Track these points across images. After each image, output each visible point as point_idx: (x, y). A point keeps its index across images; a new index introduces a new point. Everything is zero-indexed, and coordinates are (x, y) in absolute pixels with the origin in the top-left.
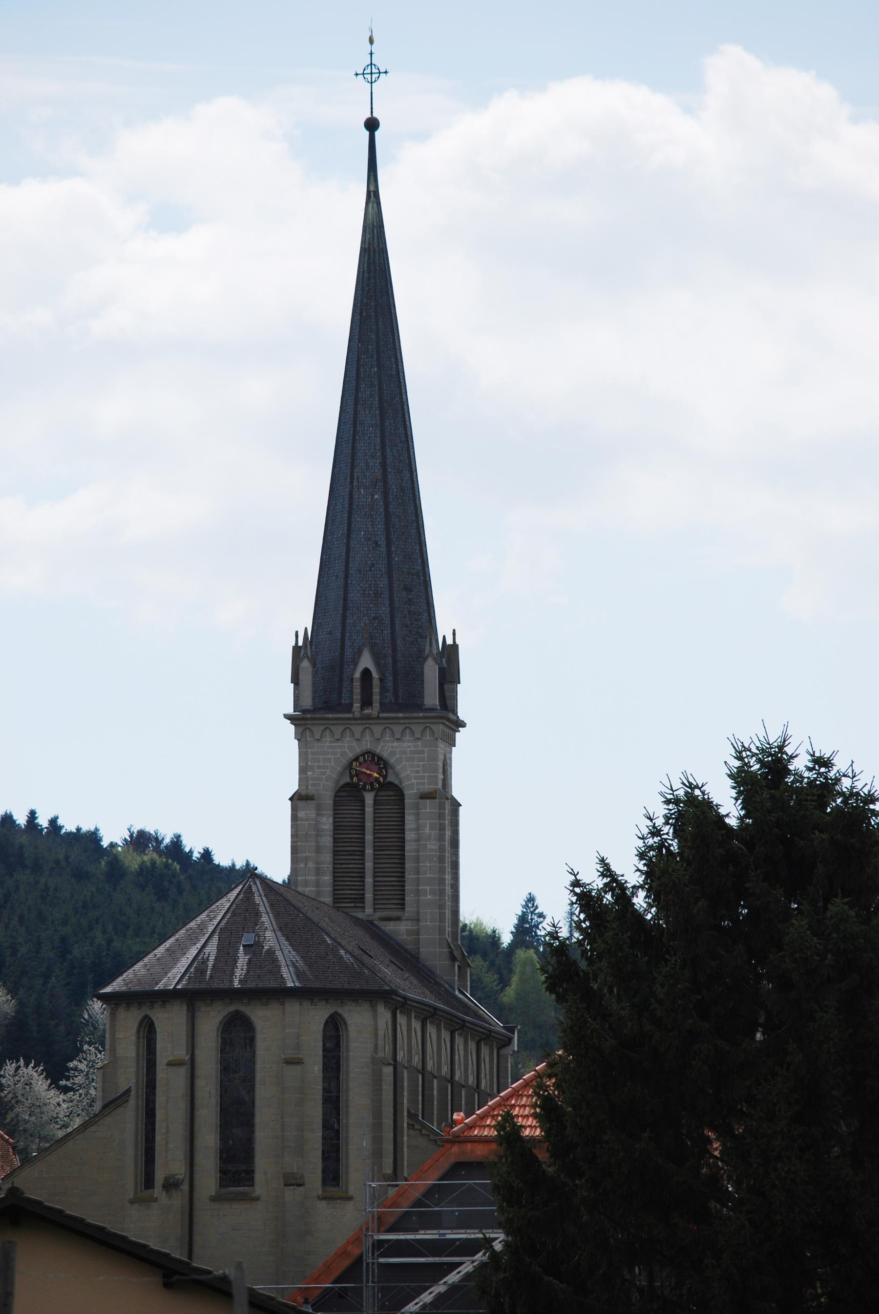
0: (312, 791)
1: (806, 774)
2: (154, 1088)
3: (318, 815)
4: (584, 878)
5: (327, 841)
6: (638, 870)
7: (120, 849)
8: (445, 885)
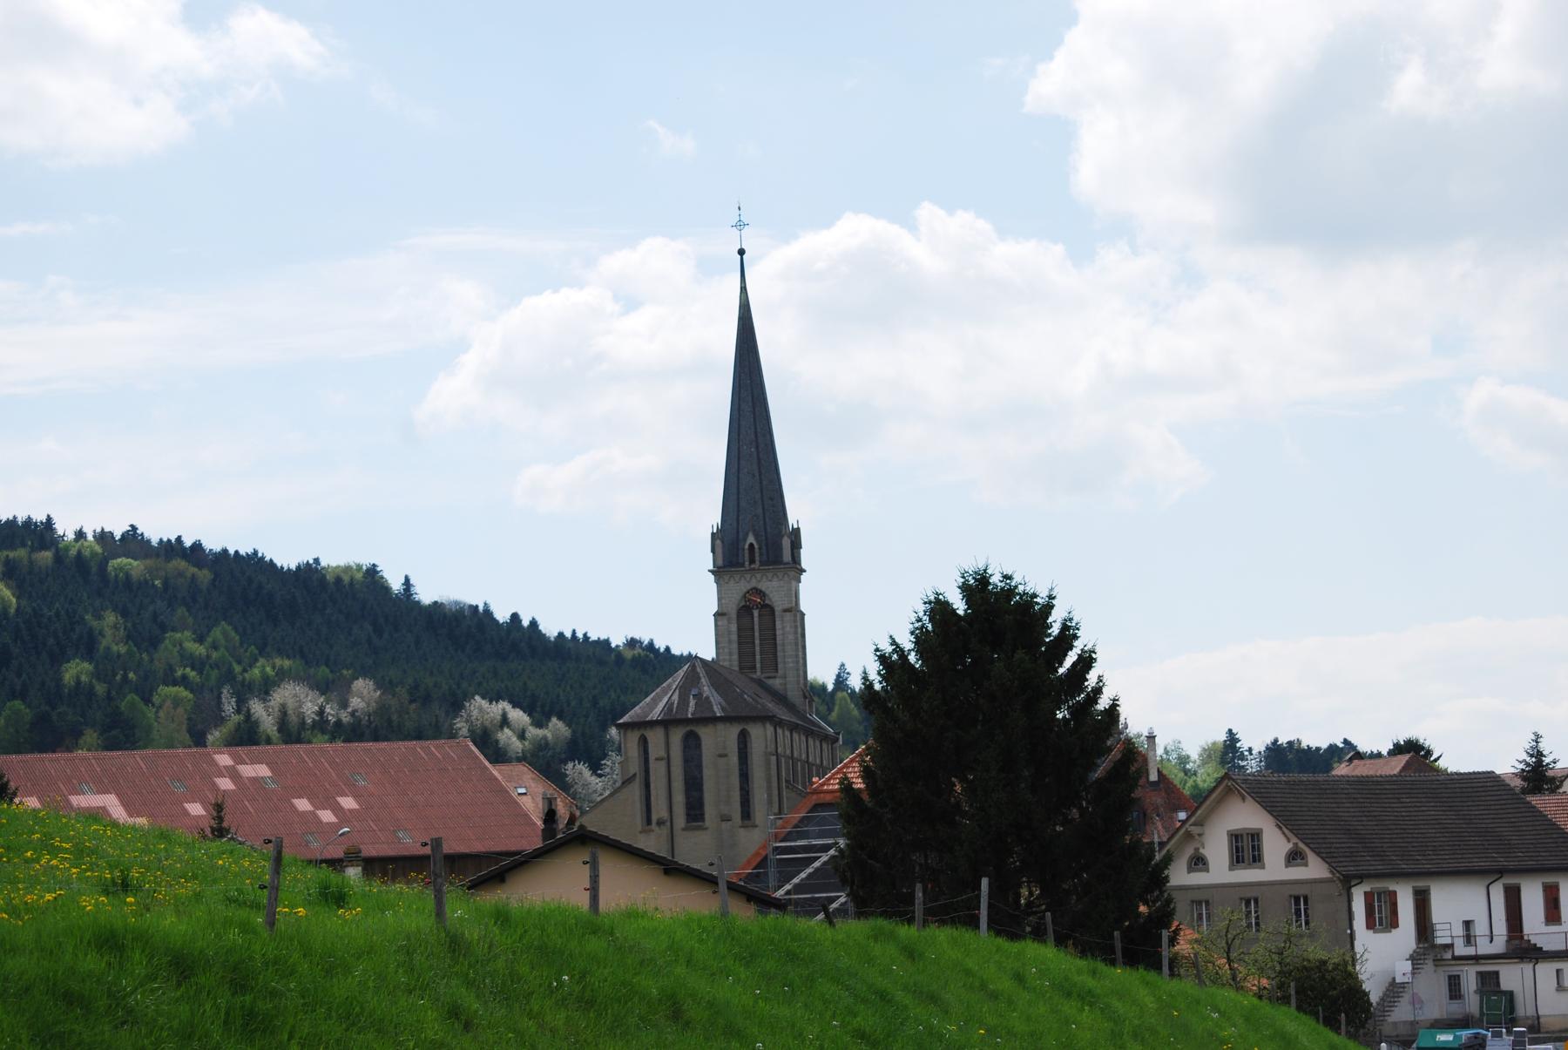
4: (881, 647)
5: (734, 637)
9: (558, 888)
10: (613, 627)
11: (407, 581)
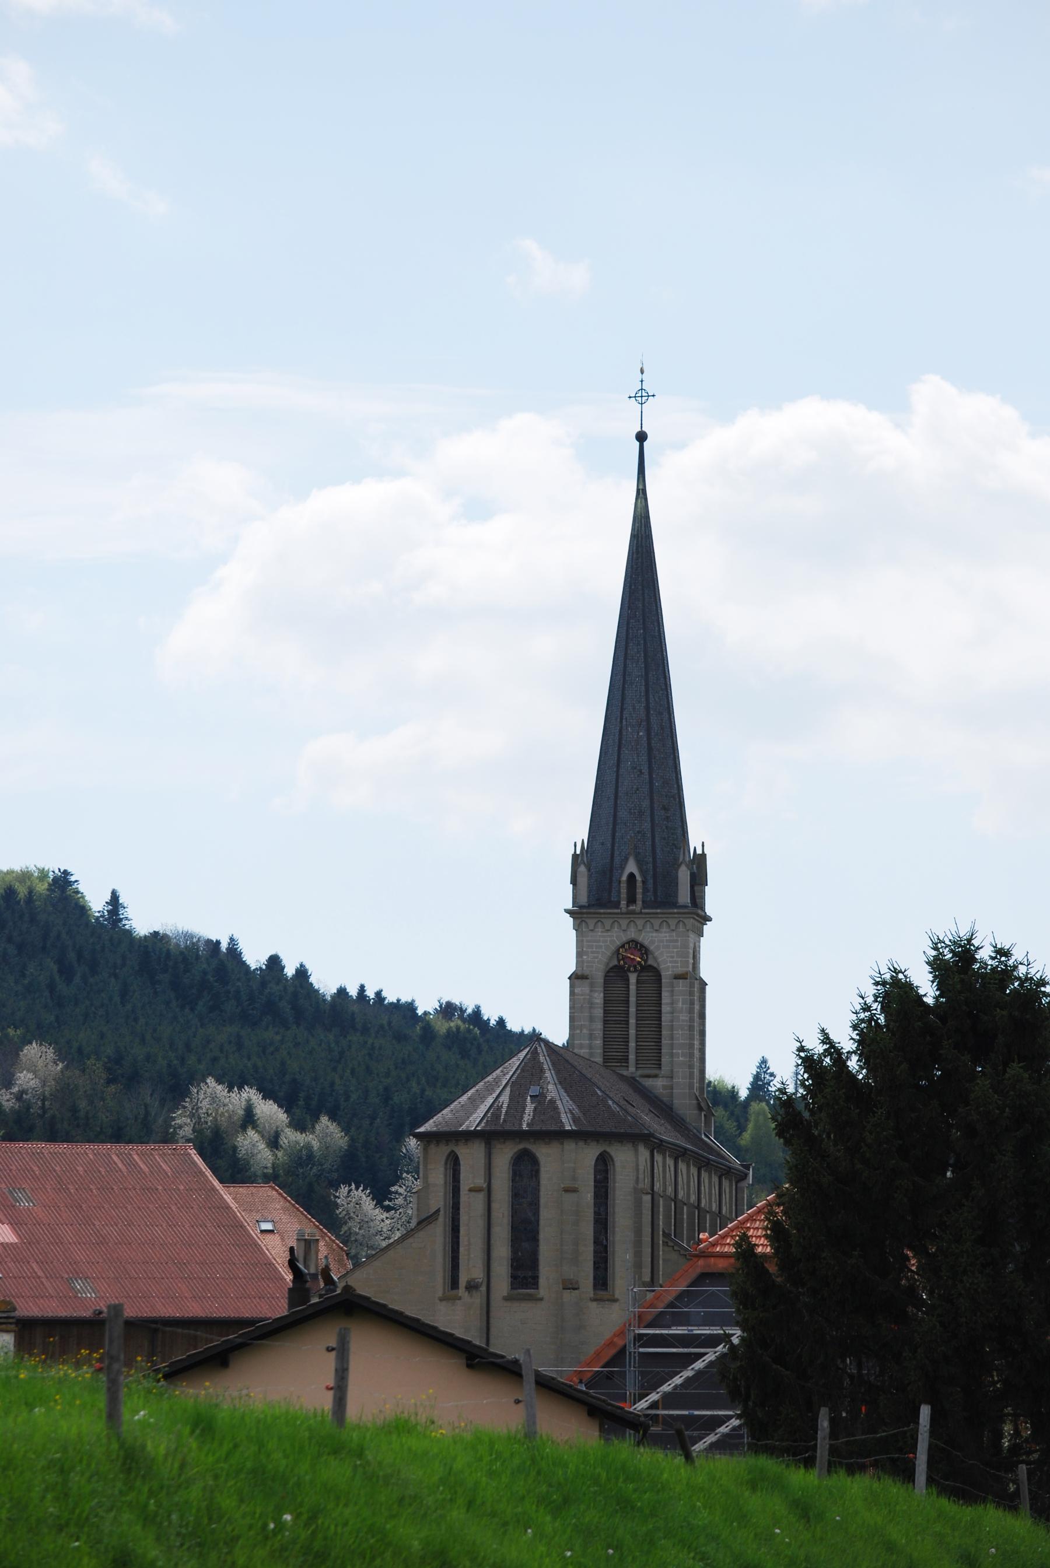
0: (587, 972)
1: (990, 962)
3: (591, 991)
4: (808, 1045)
5: (599, 1012)
6: (852, 1039)
9: (287, 1386)
10: (419, 979)
11: (115, 899)
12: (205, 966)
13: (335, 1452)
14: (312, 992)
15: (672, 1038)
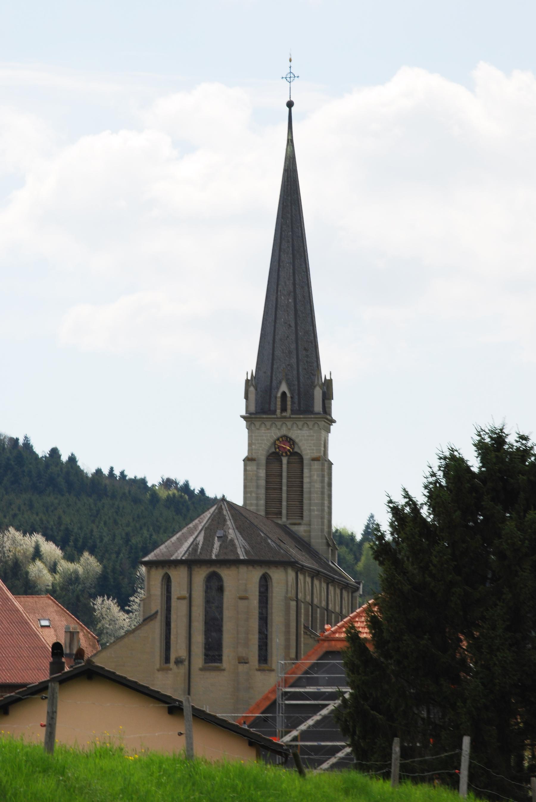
0: (254, 456)
1: (515, 444)
2: (170, 611)
3: (258, 469)
5: (263, 483)
6: (424, 495)
7: (157, 488)
8: (324, 506)
12: (8, 455)
13: (45, 771)
14: (79, 472)
15: (310, 499)
